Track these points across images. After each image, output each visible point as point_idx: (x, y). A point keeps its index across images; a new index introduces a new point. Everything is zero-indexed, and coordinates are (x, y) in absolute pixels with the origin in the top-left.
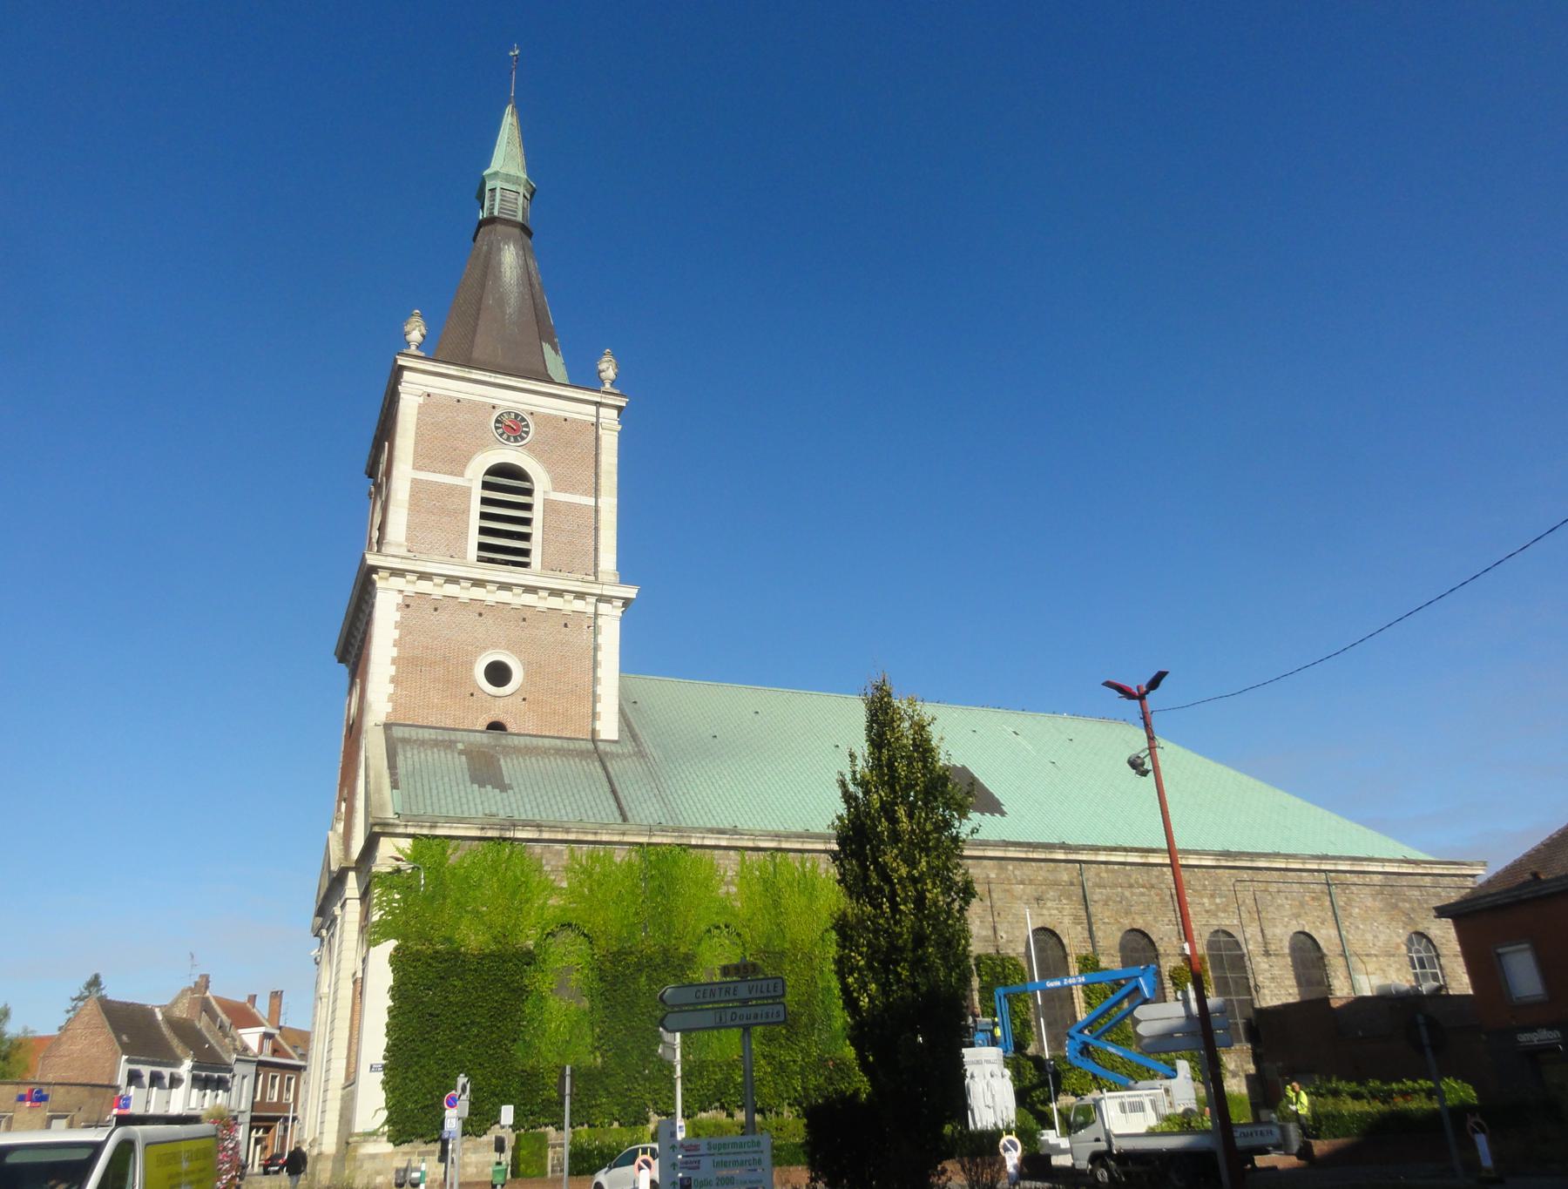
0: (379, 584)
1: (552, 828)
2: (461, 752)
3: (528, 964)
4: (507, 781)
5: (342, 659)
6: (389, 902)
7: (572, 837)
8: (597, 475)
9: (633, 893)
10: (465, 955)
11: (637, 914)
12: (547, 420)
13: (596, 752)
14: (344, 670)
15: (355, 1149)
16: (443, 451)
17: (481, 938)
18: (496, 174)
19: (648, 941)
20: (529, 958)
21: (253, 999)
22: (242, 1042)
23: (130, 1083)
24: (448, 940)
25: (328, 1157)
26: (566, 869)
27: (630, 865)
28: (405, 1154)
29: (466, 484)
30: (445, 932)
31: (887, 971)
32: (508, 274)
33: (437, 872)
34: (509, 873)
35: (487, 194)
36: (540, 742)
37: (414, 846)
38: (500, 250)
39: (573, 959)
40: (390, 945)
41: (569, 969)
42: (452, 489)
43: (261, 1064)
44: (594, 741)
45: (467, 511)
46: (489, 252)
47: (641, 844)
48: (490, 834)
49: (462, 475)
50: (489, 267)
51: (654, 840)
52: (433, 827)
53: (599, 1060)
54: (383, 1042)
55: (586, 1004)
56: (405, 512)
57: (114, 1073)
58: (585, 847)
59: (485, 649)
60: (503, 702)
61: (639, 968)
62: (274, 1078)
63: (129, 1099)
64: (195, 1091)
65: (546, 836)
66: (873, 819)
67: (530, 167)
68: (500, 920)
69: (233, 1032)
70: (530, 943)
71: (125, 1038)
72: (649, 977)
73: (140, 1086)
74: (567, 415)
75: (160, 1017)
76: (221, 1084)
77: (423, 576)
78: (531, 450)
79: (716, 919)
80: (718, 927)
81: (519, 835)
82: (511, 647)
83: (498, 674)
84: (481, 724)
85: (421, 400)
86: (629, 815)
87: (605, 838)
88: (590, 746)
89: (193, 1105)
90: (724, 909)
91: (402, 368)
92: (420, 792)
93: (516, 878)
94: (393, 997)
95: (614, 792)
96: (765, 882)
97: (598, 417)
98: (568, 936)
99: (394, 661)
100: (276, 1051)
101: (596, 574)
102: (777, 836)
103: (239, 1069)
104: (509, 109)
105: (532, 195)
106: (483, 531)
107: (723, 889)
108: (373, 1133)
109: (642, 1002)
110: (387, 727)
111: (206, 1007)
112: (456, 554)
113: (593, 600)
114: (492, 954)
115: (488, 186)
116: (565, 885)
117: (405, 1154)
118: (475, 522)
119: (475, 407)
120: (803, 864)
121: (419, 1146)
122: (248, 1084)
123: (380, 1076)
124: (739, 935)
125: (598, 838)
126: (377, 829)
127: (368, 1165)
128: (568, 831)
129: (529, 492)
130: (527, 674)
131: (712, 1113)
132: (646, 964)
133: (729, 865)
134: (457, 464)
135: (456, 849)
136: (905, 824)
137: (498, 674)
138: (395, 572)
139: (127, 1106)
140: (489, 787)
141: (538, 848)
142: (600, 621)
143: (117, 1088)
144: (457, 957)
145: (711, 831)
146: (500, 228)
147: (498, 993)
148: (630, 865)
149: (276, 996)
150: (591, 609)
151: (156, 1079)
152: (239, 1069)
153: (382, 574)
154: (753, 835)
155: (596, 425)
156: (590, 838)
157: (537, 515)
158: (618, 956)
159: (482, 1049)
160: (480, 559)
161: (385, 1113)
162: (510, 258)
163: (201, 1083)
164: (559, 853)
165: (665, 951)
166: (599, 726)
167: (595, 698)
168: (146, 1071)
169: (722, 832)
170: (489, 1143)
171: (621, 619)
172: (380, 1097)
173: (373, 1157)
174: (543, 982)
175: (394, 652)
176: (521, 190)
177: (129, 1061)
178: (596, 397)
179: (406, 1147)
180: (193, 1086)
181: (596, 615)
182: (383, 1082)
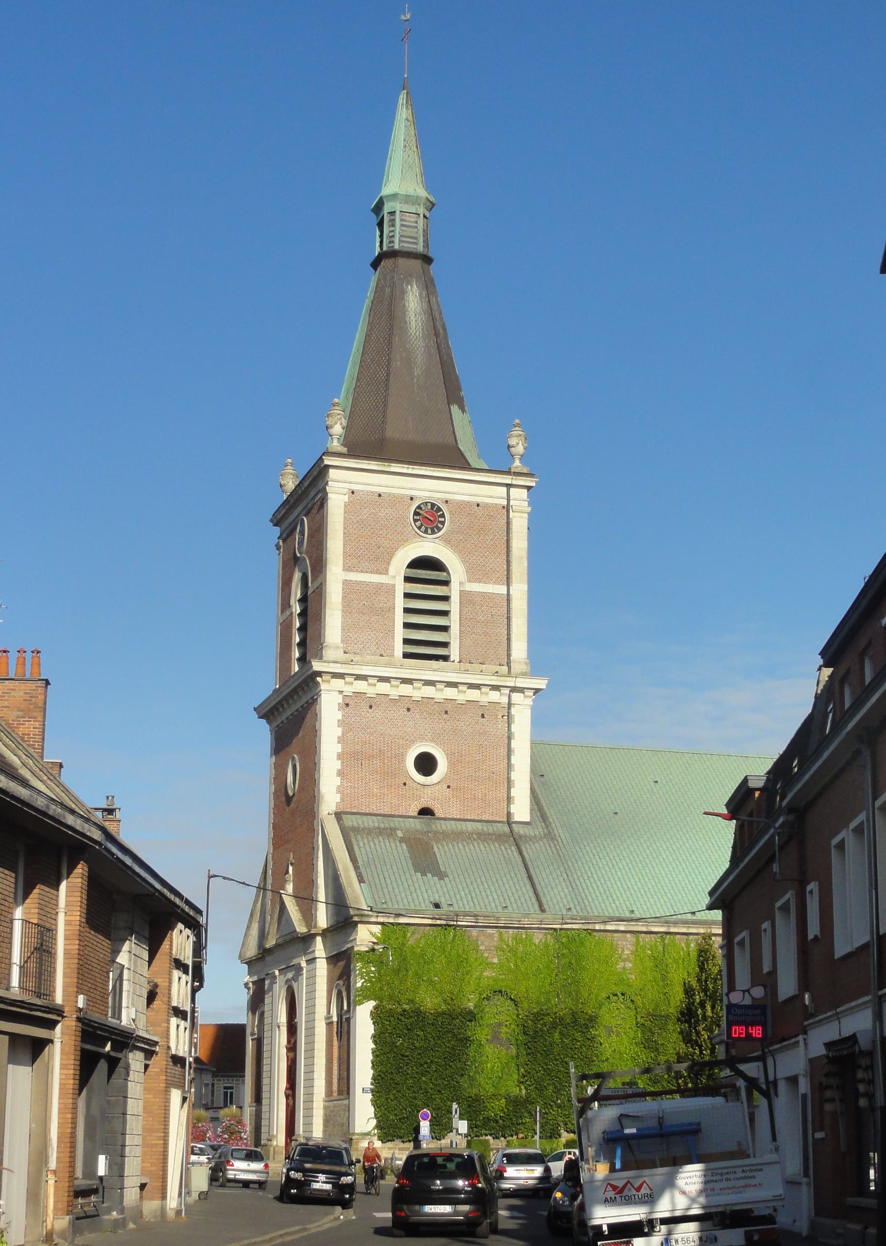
0: (323, 686)
2: (402, 840)
3: (471, 1021)
4: (443, 869)
6: (368, 973)
8: (508, 562)
9: (548, 967)
11: (551, 984)
12: (462, 507)
13: (510, 835)
16: (369, 553)
17: (435, 1001)
19: (561, 1006)
20: (471, 1016)
24: (412, 1001)
26: (497, 948)
27: (547, 946)
28: (389, 1148)
29: (391, 582)
31: (697, 1079)
33: (400, 951)
34: (454, 952)
36: (463, 826)
37: (383, 930)
38: (403, 292)
39: (502, 1018)
40: (370, 1005)
41: (500, 1025)
42: (379, 588)
44: (509, 823)
47: (555, 929)
48: (438, 922)
49: (386, 572)
53: (524, 1092)
54: (371, 1073)
55: (513, 1051)
58: (511, 931)
59: (413, 742)
61: (554, 1025)
66: (696, 1007)
67: (429, 179)
68: (447, 988)
70: (471, 1005)
74: (479, 500)
77: (359, 677)
78: (447, 541)
79: (615, 989)
80: (616, 995)
82: (435, 739)
83: (426, 764)
84: (414, 811)
86: (546, 906)
88: (506, 829)
90: (621, 981)
92: (377, 880)
93: (459, 956)
94: (375, 1042)
95: (530, 878)
98: (498, 1000)
99: (339, 756)
101: (509, 664)
106: (407, 626)
107: (621, 965)
108: (368, 1134)
109: (556, 1050)
110: (338, 815)
112: (384, 653)
113: (507, 691)
114: (443, 1013)
115: (387, 209)
116: (496, 961)
117: (389, 1148)
118: (400, 618)
119: (396, 500)
120: (688, 946)
123: (369, 1096)
129: (446, 583)
130: (451, 764)
133: (627, 946)
134: (381, 564)
135: (413, 933)
136: (709, 1013)
137: (426, 764)
138: (336, 675)
140: (429, 875)
141: (474, 932)
142: (513, 711)
144: (418, 1015)
146: (402, 262)
147: (449, 1041)
148: (547, 946)
150: (505, 700)
153: (325, 677)
155: (507, 508)
157: (454, 605)
158: (538, 1016)
159: (439, 1082)
160: (406, 656)
164: (491, 936)
165: (574, 1014)
167: (509, 783)
171: (533, 708)
172: (370, 1111)
174: (481, 1034)
175: (339, 748)
178: (507, 480)
179: (389, 1144)
181: (510, 704)
182: (372, 1100)
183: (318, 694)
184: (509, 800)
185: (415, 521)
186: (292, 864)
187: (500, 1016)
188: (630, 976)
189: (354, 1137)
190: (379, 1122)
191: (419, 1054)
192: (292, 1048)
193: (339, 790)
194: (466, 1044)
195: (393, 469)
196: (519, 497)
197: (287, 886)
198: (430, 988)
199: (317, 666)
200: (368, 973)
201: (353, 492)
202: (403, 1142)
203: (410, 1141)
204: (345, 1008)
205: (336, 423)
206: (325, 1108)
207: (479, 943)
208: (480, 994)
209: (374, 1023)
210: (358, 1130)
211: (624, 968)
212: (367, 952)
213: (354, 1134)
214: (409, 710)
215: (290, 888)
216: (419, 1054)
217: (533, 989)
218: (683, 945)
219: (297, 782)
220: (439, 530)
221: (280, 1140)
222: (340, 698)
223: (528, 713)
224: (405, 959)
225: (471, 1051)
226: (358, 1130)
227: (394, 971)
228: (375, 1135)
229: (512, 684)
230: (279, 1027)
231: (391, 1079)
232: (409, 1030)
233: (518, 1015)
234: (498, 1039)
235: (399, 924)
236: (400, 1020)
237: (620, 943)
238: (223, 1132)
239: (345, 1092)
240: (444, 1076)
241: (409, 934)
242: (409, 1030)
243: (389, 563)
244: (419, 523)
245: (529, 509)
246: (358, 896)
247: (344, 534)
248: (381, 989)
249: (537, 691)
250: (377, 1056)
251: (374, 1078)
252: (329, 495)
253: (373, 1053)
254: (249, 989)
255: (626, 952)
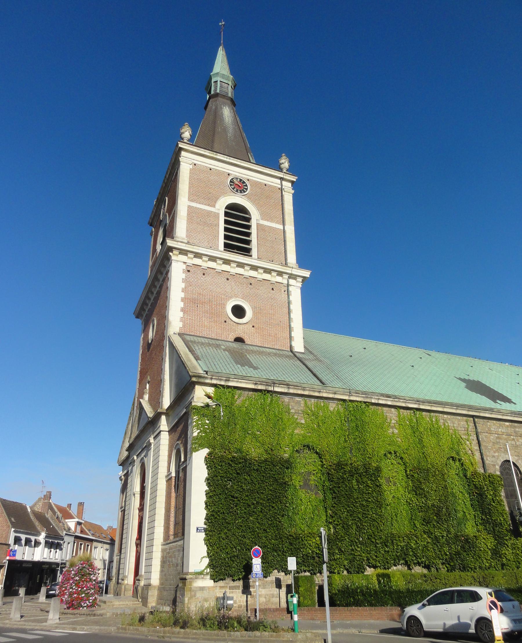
0: (173, 258)
1: (296, 386)
3: (287, 468)
5: (138, 316)
7: (306, 393)
8: (283, 214)
9: (342, 429)
10: (251, 459)
12: (256, 184)
14: (139, 323)
15: (191, 583)
17: (258, 451)
18: (217, 74)
19: (356, 460)
20: (288, 464)
21: (70, 506)
22: (67, 525)
23: (15, 544)
24: (240, 451)
25: (155, 587)
27: (339, 413)
28: (221, 587)
29: (217, 211)
30: (237, 445)
32: (227, 119)
33: (229, 407)
35: (213, 84)
36: (264, 349)
37: (216, 393)
38: (221, 108)
39: (311, 468)
40: (205, 452)
42: (209, 214)
43: (77, 537)
45: (218, 225)
46: (216, 108)
47: (344, 400)
48: (260, 387)
49: (214, 206)
50: (217, 116)
51: (352, 398)
52: (227, 380)
56: (185, 222)
57: (7, 537)
58: (313, 400)
60: (243, 327)
62: (81, 544)
63: (15, 551)
64: (46, 549)
65: (291, 391)
69: (63, 520)
71: (13, 519)
72: (358, 481)
73: (20, 545)
75: (29, 510)
76: (58, 546)
77: (198, 255)
80: (390, 453)
81: (277, 389)
83: (239, 312)
84: (231, 338)
85: (191, 167)
87: (325, 395)
89: (45, 556)
91: (181, 149)
94: (209, 485)
96: (412, 427)
97: (282, 185)
99: (182, 300)
100: (82, 532)
102: (418, 401)
103: (67, 539)
104: (221, 48)
105: (235, 87)
107: (390, 431)
108: (201, 573)
111: (50, 507)
114: (266, 460)
116: (303, 421)
117: (221, 587)
119: (219, 173)
121: (229, 582)
122: (70, 546)
123: (203, 535)
124: (402, 458)
125: (321, 395)
126: (194, 379)
127: (199, 595)
128: (304, 389)
130: (254, 313)
131: (399, 567)
132: (354, 472)
134: (212, 202)
135: (240, 396)
138: (183, 252)
139: (14, 555)
140: (247, 367)
141: (286, 399)
142: (291, 288)
143: (9, 545)
145: (382, 395)
146: (220, 99)
148: (339, 413)
149: (81, 504)
150: (285, 282)
151: (28, 542)
152: (67, 539)
154: (406, 400)
156: (317, 394)
157: (254, 230)
158: (339, 466)
161: (207, 561)
162: (227, 113)
163: (50, 545)
164: (298, 403)
166: (293, 344)
168: (23, 537)
169: (388, 396)
170: (271, 582)
171: (302, 289)
172: (203, 550)
173: (202, 589)
175: (183, 295)
176: (230, 83)
177: (15, 532)
178: (281, 175)
179: (221, 583)
180: (45, 546)
182: (205, 540)
183: (171, 263)
184: (291, 338)
185: (231, 185)
186: (148, 383)
187: (307, 465)
188: (397, 439)
189: (188, 577)
190: (211, 560)
191: (247, 496)
192: (141, 509)
193: (182, 319)
194: (285, 488)
195: (218, 157)
196: (287, 186)
197: (145, 396)
198: (254, 440)
199: (170, 243)
200: (203, 425)
201: (195, 165)
202: (234, 580)
203: (239, 579)
204: (182, 460)
205: (186, 131)
206: (163, 551)
207: (290, 407)
208: (293, 447)
209: (207, 468)
210: (191, 569)
211: (393, 433)
212: (203, 407)
213: (187, 574)
214: (228, 279)
215: (146, 397)
216: (247, 496)
217: (332, 445)
218: (428, 419)
219: (155, 331)
220: (245, 192)
221: (130, 580)
222: (184, 267)
223: (299, 291)
224: (233, 415)
225: (290, 491)
226: (191, 569)
227: (224, 424)
228: (207, 574)
229: (290, 272)
230: (134, 495)
231: (223, 518)
232: (238, 474)
233: (322, 466)
234: (308, 485)
235: (229, 387)
236: (230, 465)
237: (388, 414)
238: (75, 575)
239: (180, 534)
240: (268, 516)
241: (236, 397)
242: (238, 474)
243: (215, 202)
244: (233, 187)
245: (293, 192)
246: (196, 367)
247: (189, 183)
248: (214, 438)
249: (304, 278)
250: (210, 497)
251: (207, 519)
252: (181, 163)
253: (206, 494)
254: (121, 480)
255: (393, 421)
